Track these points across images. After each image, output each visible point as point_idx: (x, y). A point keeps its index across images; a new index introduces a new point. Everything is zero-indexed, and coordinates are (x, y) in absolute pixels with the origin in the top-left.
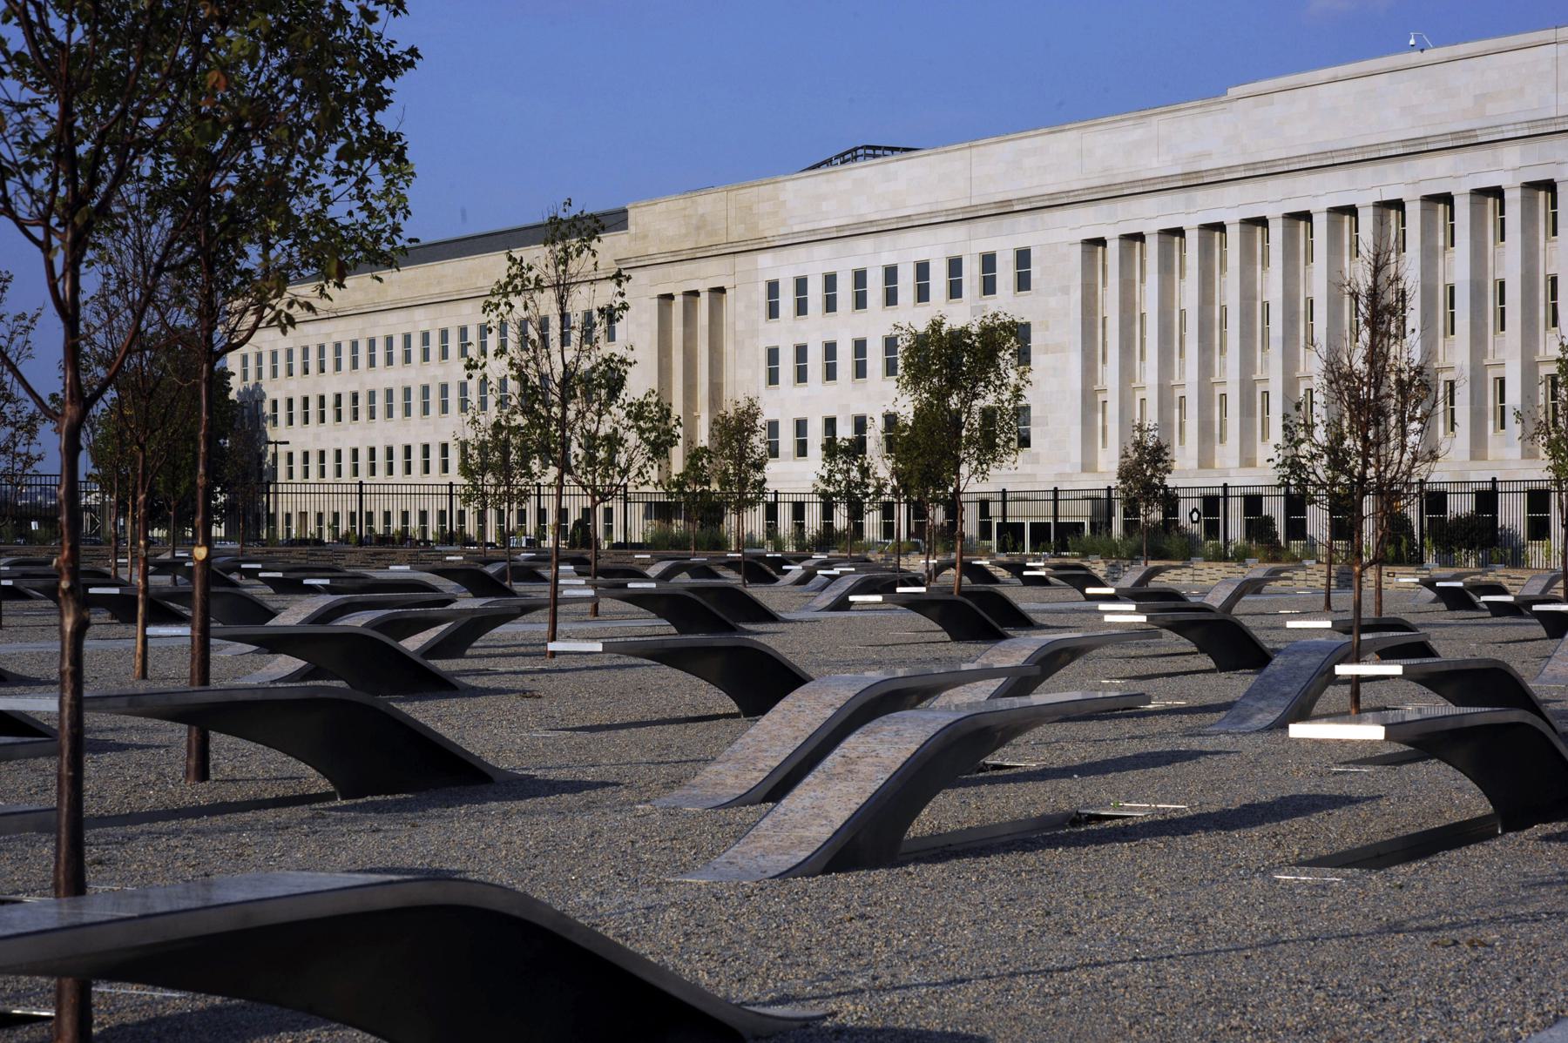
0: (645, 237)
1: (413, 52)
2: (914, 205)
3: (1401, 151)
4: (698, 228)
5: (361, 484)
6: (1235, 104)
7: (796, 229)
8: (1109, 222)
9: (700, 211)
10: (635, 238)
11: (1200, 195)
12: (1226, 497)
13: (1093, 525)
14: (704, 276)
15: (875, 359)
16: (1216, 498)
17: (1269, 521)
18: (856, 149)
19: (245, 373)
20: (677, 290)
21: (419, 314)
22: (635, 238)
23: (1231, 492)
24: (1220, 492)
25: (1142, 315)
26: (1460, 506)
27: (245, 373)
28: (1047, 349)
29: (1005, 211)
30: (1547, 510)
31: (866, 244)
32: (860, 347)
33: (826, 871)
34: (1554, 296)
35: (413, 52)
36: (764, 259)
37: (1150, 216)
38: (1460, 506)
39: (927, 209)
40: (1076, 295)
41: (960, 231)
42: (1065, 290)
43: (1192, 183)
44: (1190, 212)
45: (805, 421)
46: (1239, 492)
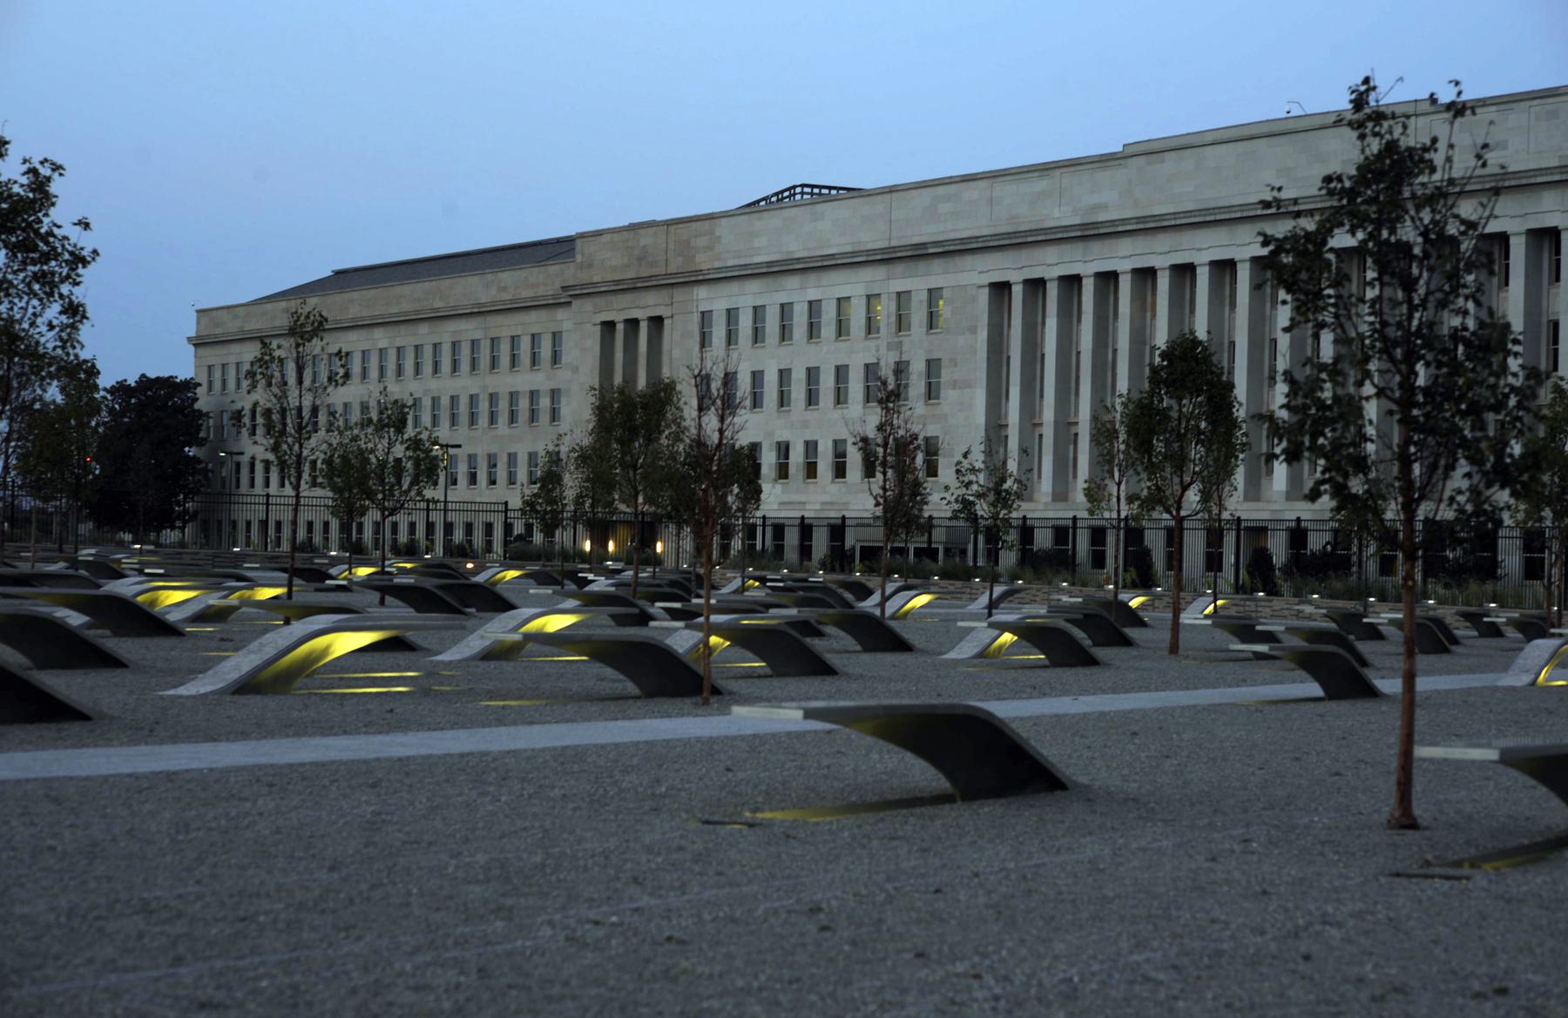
0: (591, 265)
1: (95, 252)
2: (838, 244)
3: (1239, 215)
4: (640, 259)
5: (268, 496)
6: (1130, 161)
7: (730, 263)
8: (1014, 269)
9: (643, 242)
10: (581, 267)
11: (1096, 247)
12: (1075, 528)
13: (947, 550)
14: (643, 307)
15: (856, 387)
16: (1067, 528)
17: (1147, 553)
18: (794, 187)
19: (210, 383)
20: (618, 317)
21: (378, 333)
22: (581, 267)
23: (1079, 524)
24: (1070, 523)
25: (1079, 353)
26: (1043, 540)
27: (210, 383)
28: (954, 385)
29: (919, 254)
30: (1104, 544)
31: (793, 282)
32: (841, 372)
33: (234, 693)
34: (1556, 341)
35: (95, 252)
36: (702, 292)
37: (1052, 264)
38: (1043, 540)
39: (849, 249)
40: (983, 335)
41: (880, 272)
42: (973, 330)
43: (1090, 233)
44: (1087, 262)
45: (816, 443)
46: (1086, 524)
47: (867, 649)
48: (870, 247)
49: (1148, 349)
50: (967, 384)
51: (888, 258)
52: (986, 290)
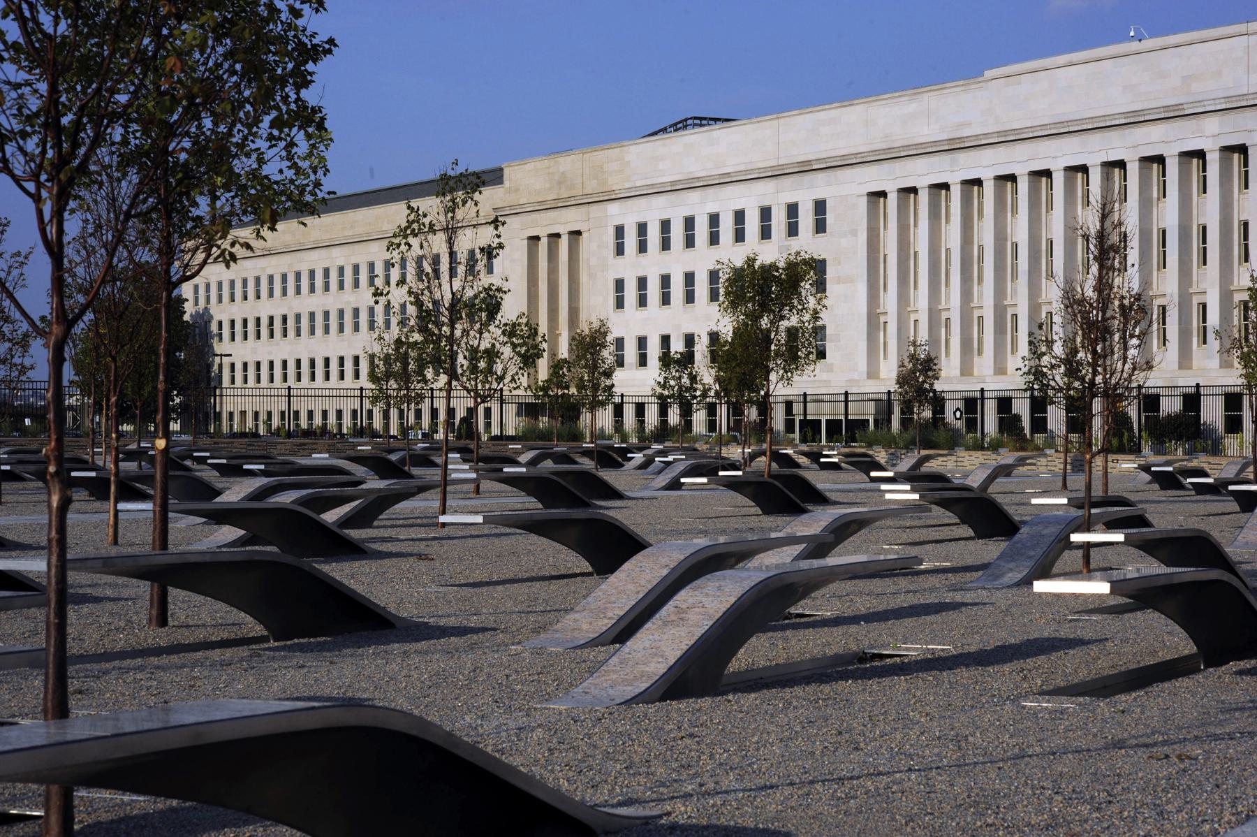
0: (517, 190)
2: (732, 165)
4: (560, 183)
5: (289, 388)
6: (990, 83)
7: (638, 184)
8: (889, 178)
9: (561, 169)
11: (962, 157)
12: (983, 398)
13: (876, 421)
14: (564, 222)
15: (702, 288)
16: (975, 399)
17: (1018, 418)
18: (686, 120)
19: (196, 299)
20: (543, 233)
21: (336, 252)
23: (987, 395)
24: (978, 395)
25: (916, 253)
26: (1171, 406)
27: (196, 299)
28: (839, 280)
29: (805, 169)
30: (1240, 409)
31: (694, 196)
34: (1246, 237)
36: (613, 208)
37: (922, 173)
38: (1171, 406)
39: (743, 168)
40: (863, 237)
41: (770, 185)
42: (854, 233)
43: (955, 147)
44: (954, 171)
45: (645, 338)
46: (993, 395)
47: (767, 512)
48: (760, 165)
49: (1009, 244)
50: (849, 280)
51: (777, 174)
52: (1137, 163)
